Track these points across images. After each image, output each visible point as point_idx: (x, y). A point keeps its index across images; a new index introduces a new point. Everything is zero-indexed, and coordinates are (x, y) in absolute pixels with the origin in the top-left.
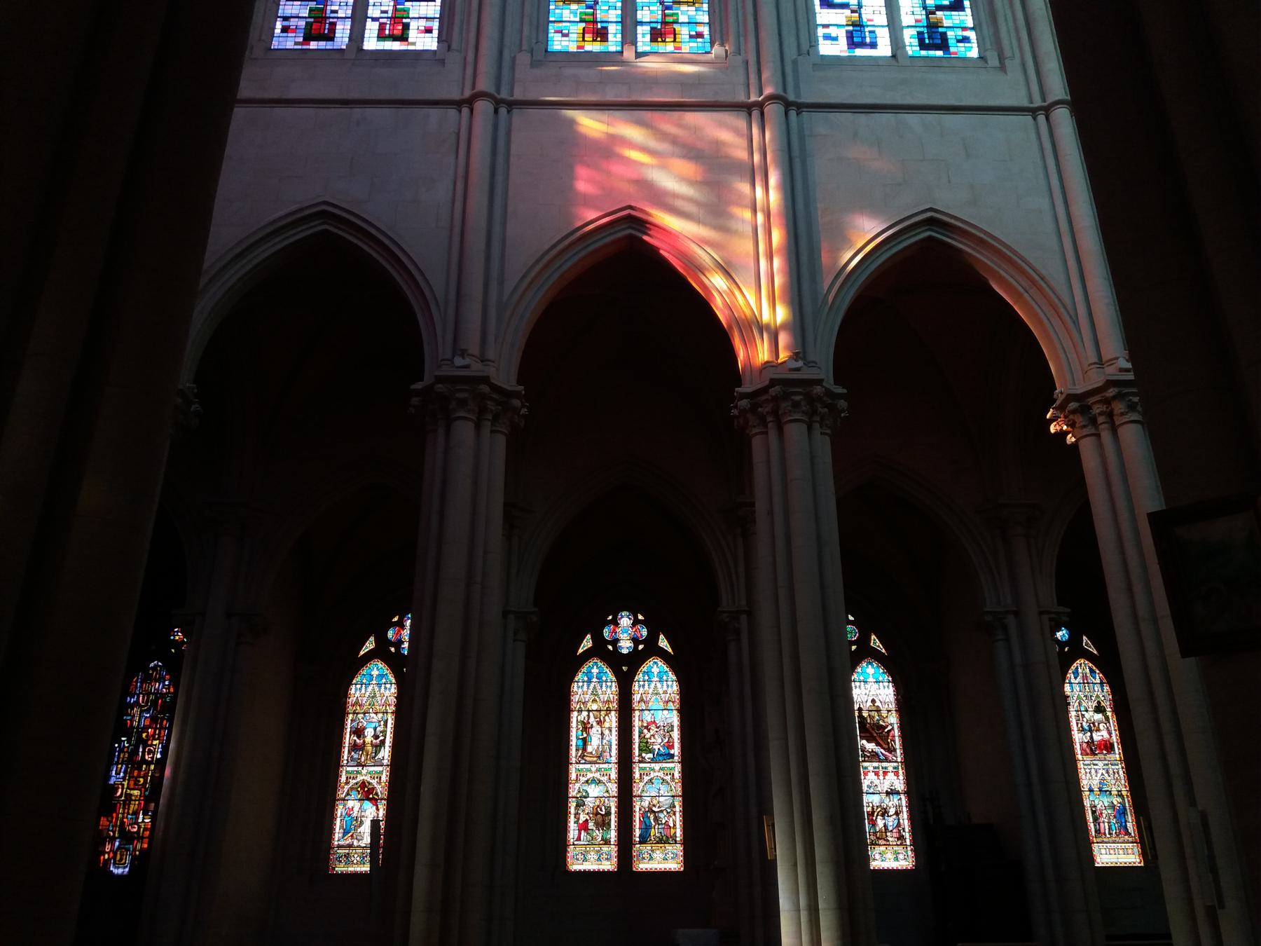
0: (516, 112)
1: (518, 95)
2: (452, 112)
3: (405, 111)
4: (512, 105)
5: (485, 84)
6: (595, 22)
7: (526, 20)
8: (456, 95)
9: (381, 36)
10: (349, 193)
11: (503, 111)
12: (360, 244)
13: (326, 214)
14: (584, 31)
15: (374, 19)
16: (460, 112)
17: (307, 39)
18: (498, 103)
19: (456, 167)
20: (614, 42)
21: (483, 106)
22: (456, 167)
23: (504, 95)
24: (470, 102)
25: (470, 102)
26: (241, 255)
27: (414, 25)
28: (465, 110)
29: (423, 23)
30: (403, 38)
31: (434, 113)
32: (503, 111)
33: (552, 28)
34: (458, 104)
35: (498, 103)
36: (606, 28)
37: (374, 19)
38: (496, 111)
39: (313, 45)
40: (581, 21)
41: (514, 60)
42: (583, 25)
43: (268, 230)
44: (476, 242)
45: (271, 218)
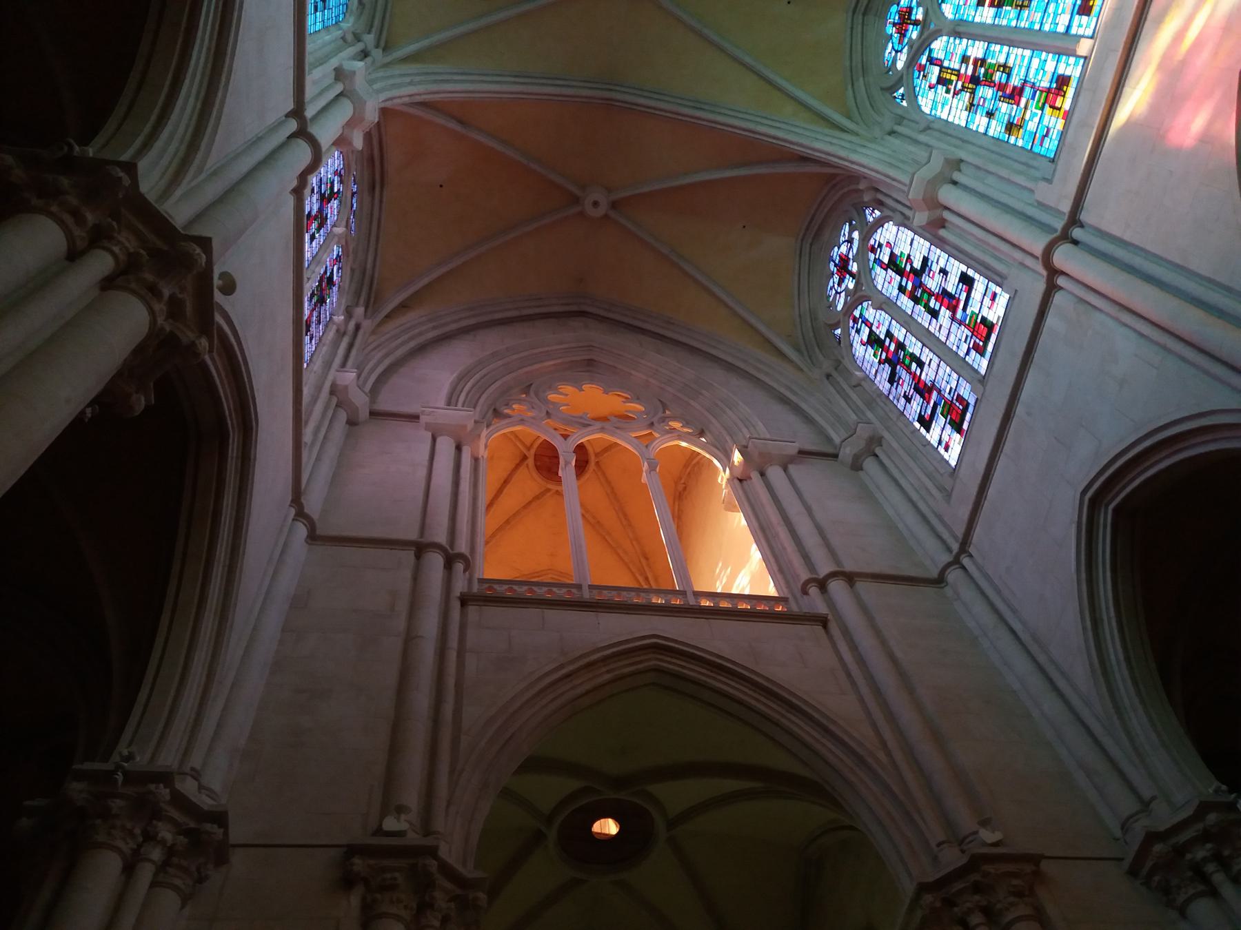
0: (1084, 217)
1: (1066, 207)
2: (1058, 298)
3: (1038, 356)
4: (1074, 220)
5: (1037, 245)
6: (1049, 90)
7: (992, 168)
8: (1041, 286)
9: (981, 351)
10: (1086, 459)
11: (1077, 233)
12: (1129, 489)
13: (1095, 500)
14: (1053, 107)
15: (968, 353)
16: (1061, 288)
17: (959, 430)
18: (1065, 237)
19: (1108, 314)
20: (1071, 67)
21: (1063, 257)
22: (1108, 314)
23: (1059, 224)
24: (1053, 272)
25: (1053, 272)
26: (1096, 623)
27: (985, 312)
28: (1061, 281)
29: (987, 301)
30: (990, 327)
31: (1051, 321)
32: (1077, 233)
33: (1037, 149)
34: (1051, 288)
35: (1065, 237)
36: (1059, 76)
37: (968, 353)
38: (1075, 242)
39: (965, 426)
40: (1042, 109)
41: (1041, 205)
42: (1047, 106)
43: (1083, 576)
44: (1191, 321)
45: (1074, 563)
